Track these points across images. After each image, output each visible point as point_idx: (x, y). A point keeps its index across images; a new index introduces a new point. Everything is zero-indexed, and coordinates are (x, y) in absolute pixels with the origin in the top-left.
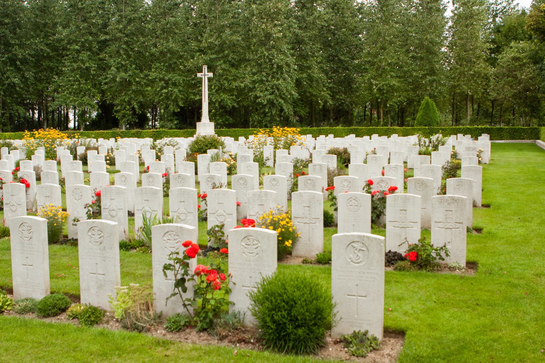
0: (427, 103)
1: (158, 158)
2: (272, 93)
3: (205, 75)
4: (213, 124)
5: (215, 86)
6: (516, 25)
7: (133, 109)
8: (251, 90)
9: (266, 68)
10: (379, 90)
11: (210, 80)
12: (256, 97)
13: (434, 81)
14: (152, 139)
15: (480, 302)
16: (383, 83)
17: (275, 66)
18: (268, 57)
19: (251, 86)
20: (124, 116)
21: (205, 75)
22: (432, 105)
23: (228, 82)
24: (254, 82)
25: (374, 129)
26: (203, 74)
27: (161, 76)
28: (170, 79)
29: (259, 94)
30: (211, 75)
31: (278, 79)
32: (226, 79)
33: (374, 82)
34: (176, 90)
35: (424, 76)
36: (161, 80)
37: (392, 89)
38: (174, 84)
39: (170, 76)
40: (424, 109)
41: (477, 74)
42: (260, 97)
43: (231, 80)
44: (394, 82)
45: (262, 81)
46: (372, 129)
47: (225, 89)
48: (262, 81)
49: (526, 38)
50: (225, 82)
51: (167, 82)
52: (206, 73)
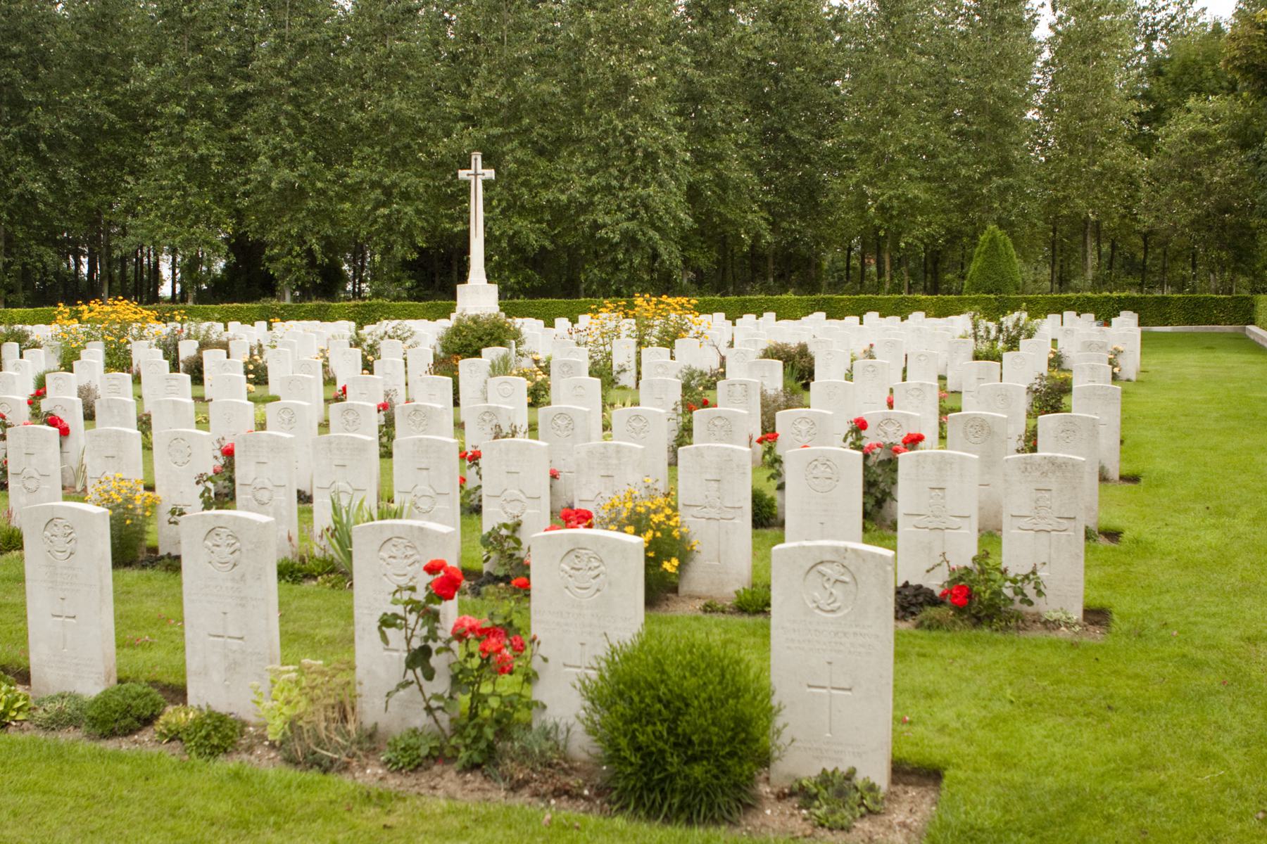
0: (993, 240)
2: (633, 217)
3: (476, 175)
4: (494, 288)
5: (499, 201)
6: (1199, 58)
7: (310, 252)
8: (584, 209)
9: (619, 158)
10: (882, 209)
11: (487, 185)
12: (596, 226)
13: (1009, 187)
16: (892, 193)
17: (640, 154)
18: (622, 133)
19: (584, 200)
20: (288, 270)
21: (476, 175)
22: (1005, 245)
24: (591, 191)
25: (870, 299)
26: (472, 171)
28: (394, 185)
29: (601, 218)
30: (490, 174)
31: (646, 185)
32: (525, 184)
33: (870, 191)
34: (409, 210)
35: (987, 176)
36: (374, 185)
37: (912, 207)
38: (405, 196)
39: (394, 176)
40: (985, 253)
41: (1110, 173)
42: (605, 226)
44: (917, 191)
45: (608, 189)
46: (864, 300)
47: (523, 206)
48: (608, 189)
49: (1222, 88)
50: (524, 190)
51: (387, 192)
52: (480, 170)
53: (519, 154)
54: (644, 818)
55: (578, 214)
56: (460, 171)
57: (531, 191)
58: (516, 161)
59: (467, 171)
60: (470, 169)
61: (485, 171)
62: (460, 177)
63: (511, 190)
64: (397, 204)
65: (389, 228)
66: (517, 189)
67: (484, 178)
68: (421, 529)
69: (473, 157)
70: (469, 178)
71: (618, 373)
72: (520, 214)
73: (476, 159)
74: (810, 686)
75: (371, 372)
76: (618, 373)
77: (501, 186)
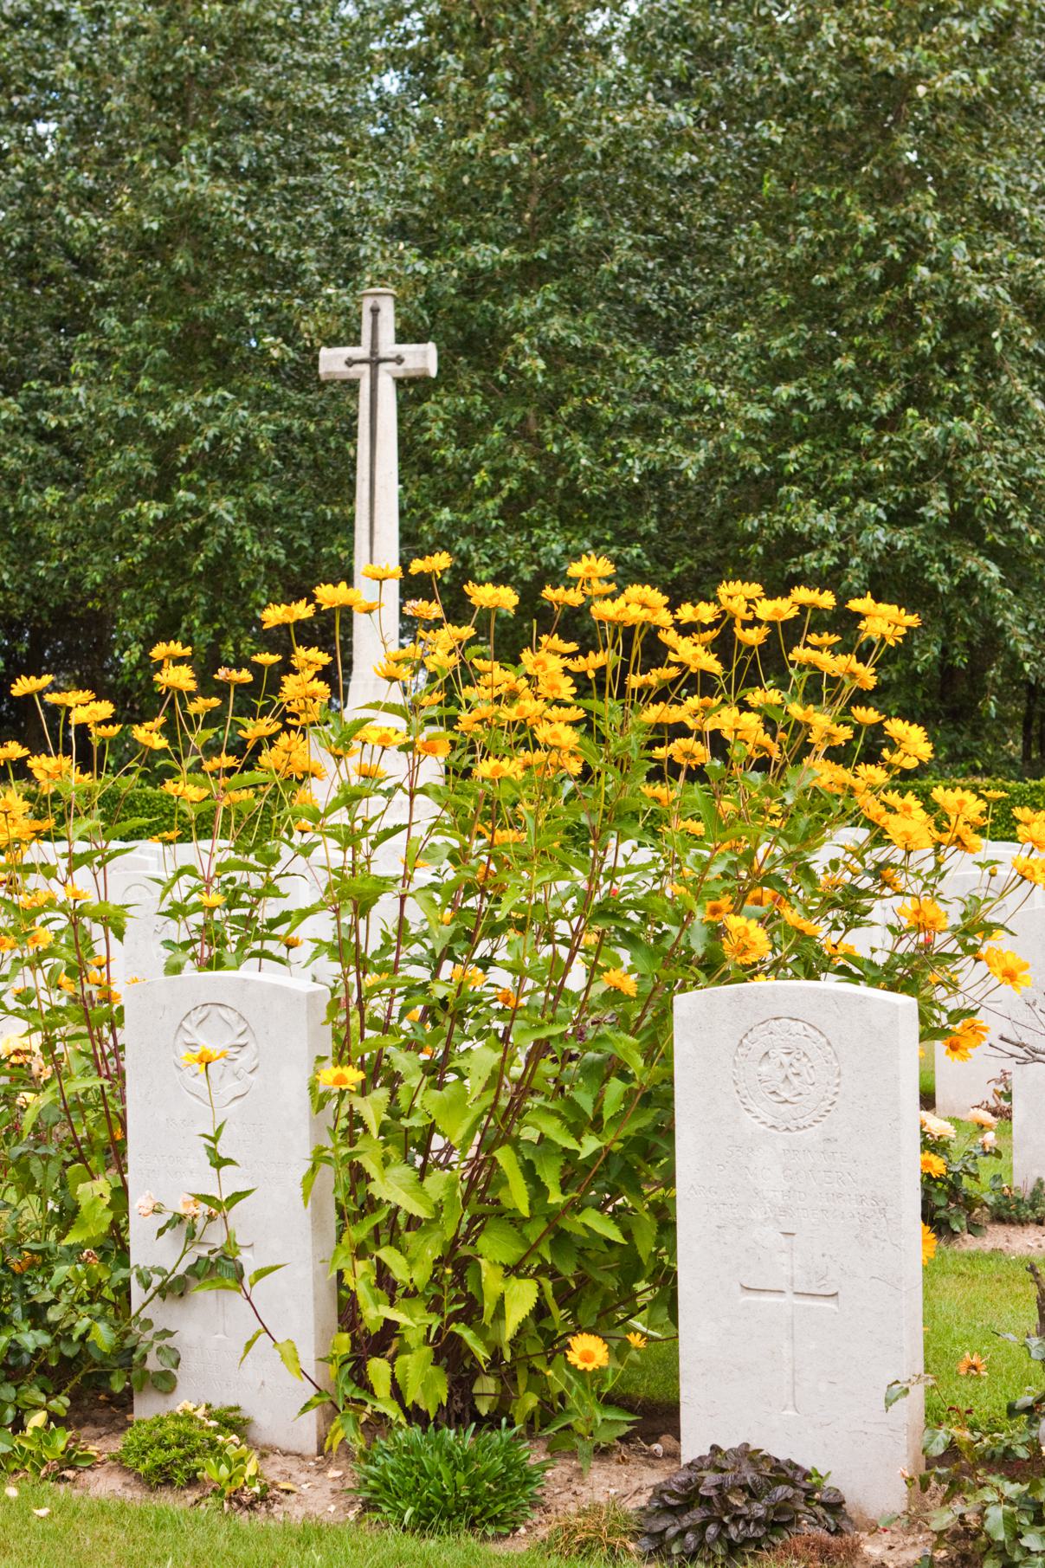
1: (340, 1274)
3: (375, 361)
5: (497, 473)
11: (413, 390)
14: (85, 867)
15: (969, 1033)
19: (754, 462)
21: (375, 361)
23: (596, 447)
26: (362, 352)
27: (124, 408)
28: (184, 431)
32: (585, 421)
34: (223, 507)
36: (126, 431)
39: (184, 406)
43: (614, 428)
47: (571, 491)
50: (577, 443)
51: (164, 446)
52: (388, 346)
53: (556, 327)
56: (324, 353)
58: (552, 351)
61: (409, 350)
62: (323, 369)
64: (190, 487)
65: (168, 560)
67: (400, 371)
68: (555, 1296)
69: (367, 304)
70: (352, 372)
71: (175, 1289)
73: (375, 311)
76: (175, 1289)
77: (507, 428)
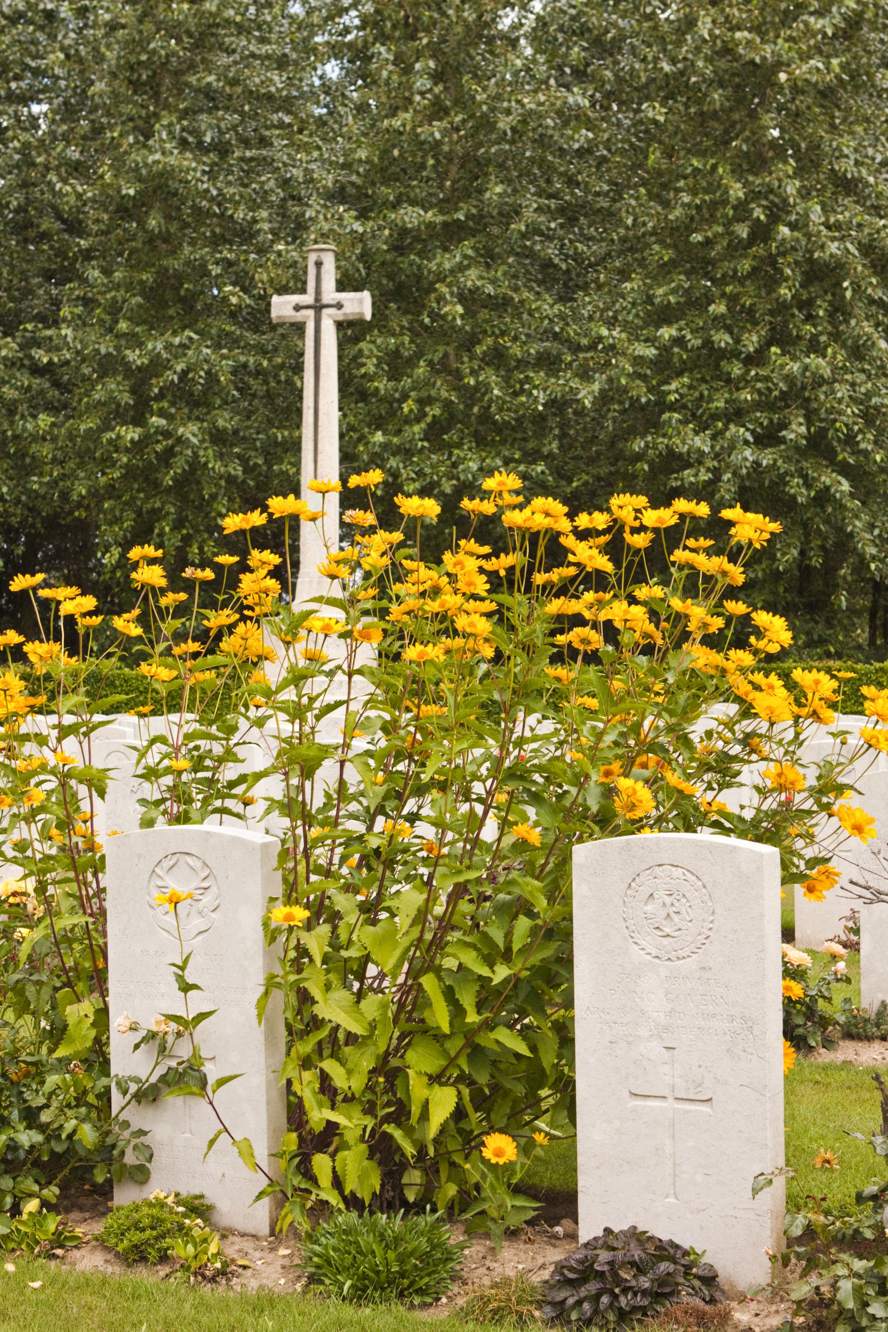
3: (318, 307)
5: (423, 402)
21: (318, 307)
26: (308, 299)
28: (156, 366)
34: (190, 431)
47: (485, 417)
52: (330, 294)
53: (472, 277)
54: (679, 593)
55: (652, 304)
56: (275, 299)
57: (507, 379)
59: (296, 299)
60: (303, 291)
61: (344, 296)
63: (458, 375)
64: (162, 414)
66: (473, 373)
67: (339, 315)
69: (312, 258)
72: (481, 442)
73: (319, 264)
74: (851, 882)
75: (139, 801)
77: (431, 363)
